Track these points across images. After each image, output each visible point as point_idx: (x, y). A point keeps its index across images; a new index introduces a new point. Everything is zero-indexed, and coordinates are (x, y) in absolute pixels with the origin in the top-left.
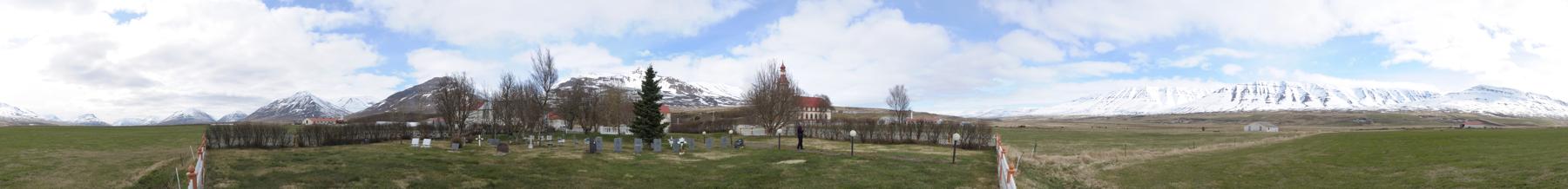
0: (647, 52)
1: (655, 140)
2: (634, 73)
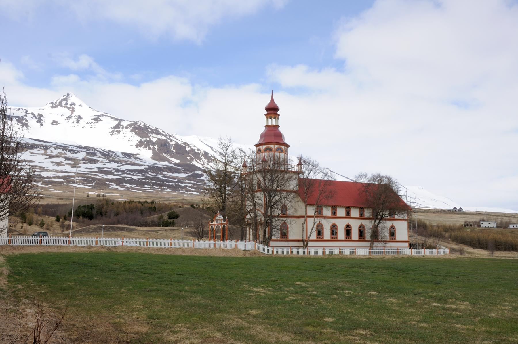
0: (85, 61)
1: (25, 126)
2: (54, 106)
